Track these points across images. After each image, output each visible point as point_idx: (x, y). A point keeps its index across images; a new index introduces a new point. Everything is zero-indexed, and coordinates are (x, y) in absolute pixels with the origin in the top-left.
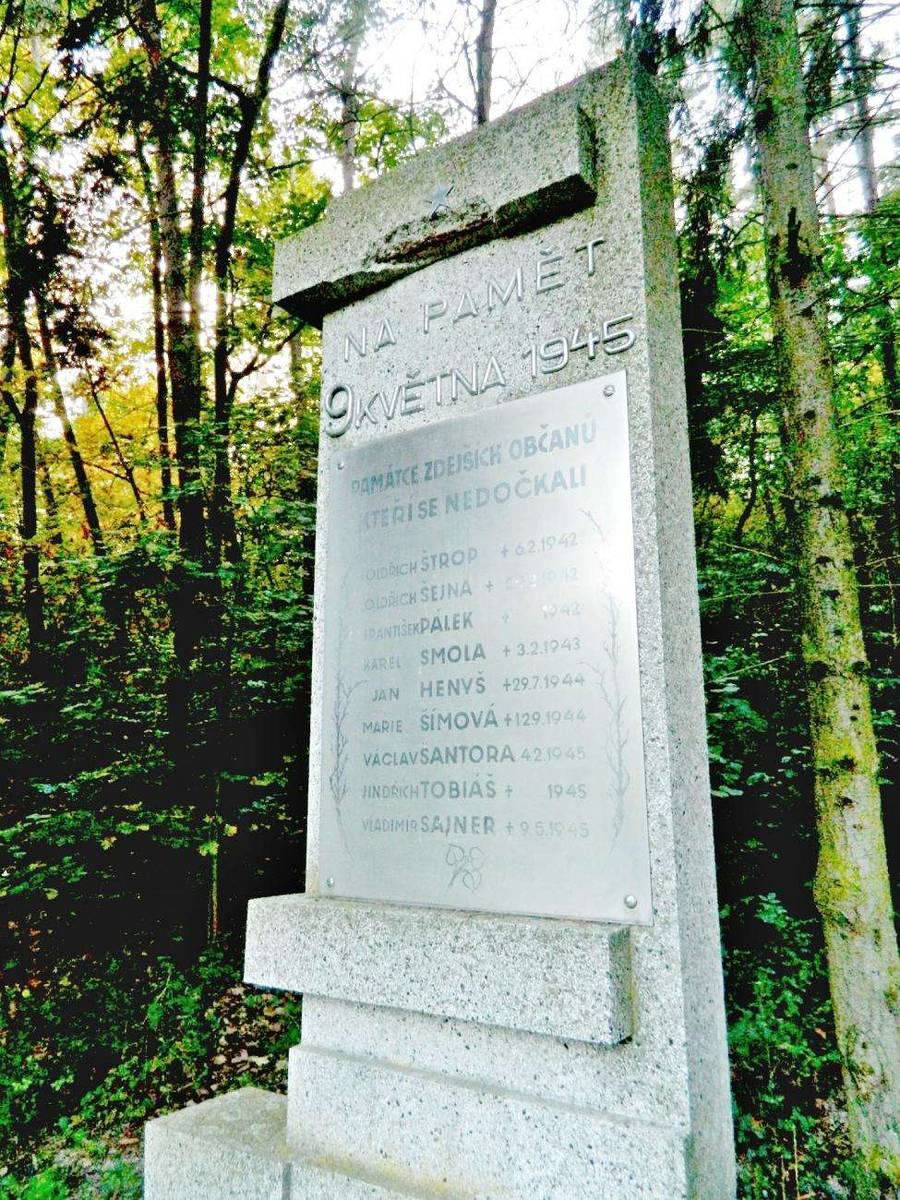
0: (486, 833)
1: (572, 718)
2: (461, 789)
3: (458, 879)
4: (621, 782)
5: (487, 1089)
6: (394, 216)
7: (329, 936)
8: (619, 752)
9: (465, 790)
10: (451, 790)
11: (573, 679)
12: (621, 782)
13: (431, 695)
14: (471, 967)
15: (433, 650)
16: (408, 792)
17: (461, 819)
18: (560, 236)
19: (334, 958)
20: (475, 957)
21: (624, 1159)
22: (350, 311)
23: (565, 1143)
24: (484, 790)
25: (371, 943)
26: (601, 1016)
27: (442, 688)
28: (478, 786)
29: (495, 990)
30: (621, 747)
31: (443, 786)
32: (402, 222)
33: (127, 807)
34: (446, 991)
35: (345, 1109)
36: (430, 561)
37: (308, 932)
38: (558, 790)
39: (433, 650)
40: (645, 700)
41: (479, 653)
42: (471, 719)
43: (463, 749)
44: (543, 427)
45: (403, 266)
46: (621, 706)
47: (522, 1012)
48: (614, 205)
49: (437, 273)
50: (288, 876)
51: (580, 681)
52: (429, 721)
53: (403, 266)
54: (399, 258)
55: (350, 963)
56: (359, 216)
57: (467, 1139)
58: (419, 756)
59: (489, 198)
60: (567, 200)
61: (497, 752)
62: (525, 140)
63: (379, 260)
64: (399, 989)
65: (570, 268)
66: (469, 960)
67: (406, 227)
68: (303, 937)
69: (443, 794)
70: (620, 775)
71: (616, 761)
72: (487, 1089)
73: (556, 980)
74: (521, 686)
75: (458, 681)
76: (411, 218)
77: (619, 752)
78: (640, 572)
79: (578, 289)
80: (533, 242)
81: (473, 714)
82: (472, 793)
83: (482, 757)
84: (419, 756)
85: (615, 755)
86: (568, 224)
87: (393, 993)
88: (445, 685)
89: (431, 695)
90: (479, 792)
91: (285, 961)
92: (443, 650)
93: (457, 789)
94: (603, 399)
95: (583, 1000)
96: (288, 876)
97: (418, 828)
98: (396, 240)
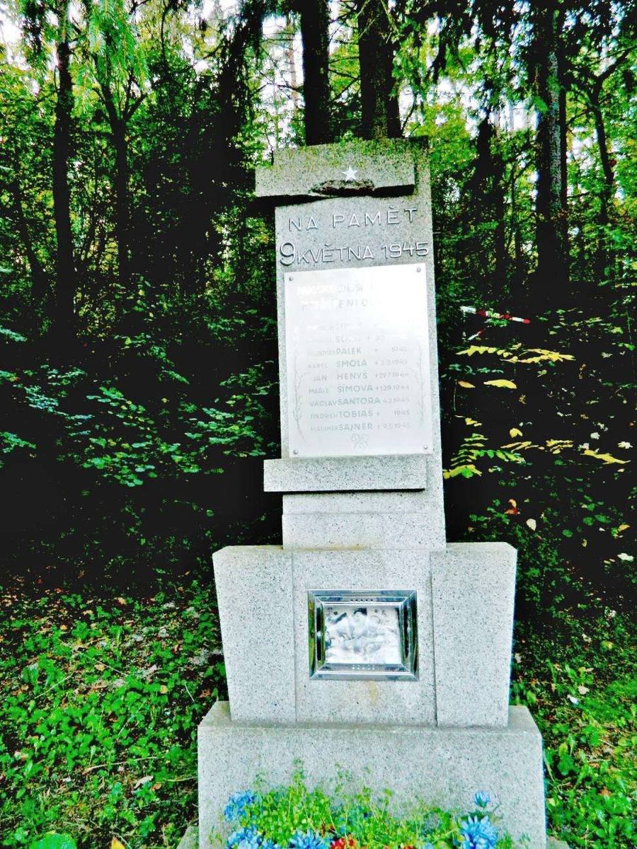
5: (371, 514)
6: (326, 174)
18: (398, 203)
19: (311, 477)
21: (425, 523)
22: (290, 208)
23: (404, 522)
32: (331, 179)
33: (569, 357)
35: (312, 531)
40: (432, 381)
41: (364, 363)
43: (358, 399)
45: (323, 196)
46: (423, 384)
48: (420, 197)
49: (338, 201)
50: (276, 453)
53: (323, 196)
54: (324, 192)
56: (306, 169)
57: (367, 530)
59: (375, 182)
60: (407, 191)
62: (391, 162)
63: (314, 191)
65: (403, 218)
66: (372, 469)
67: (332, 181)
70: (422, 407)
72: (371, 514)
76: (335, 179)
78: (430, 338)
79: (405, 227)
80: (385, 202)
86: (401, 199)
88: (349, 375)
94: (417, 273)
96: (276, 453)
98: (325, 186)
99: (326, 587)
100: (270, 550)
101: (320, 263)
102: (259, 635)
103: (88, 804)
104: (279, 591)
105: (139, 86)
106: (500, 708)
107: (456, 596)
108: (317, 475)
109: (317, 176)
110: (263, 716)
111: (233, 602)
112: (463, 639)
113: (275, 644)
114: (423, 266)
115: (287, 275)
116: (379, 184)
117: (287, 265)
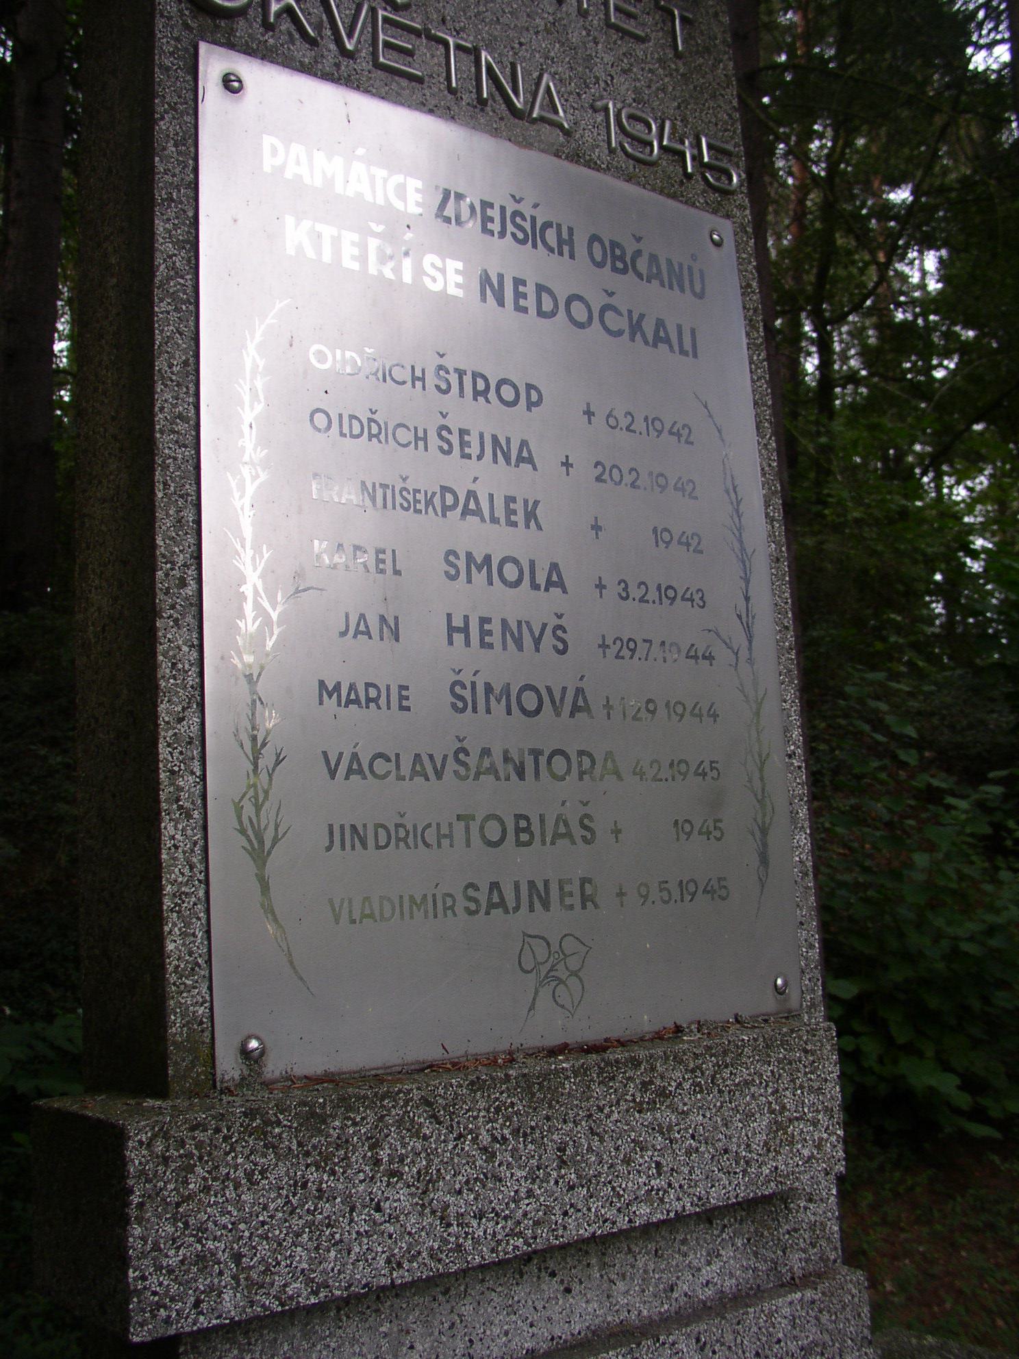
0: (584, 907)
1: (701, 716)
2: (536, 827)
3: (545, 993)
4: (764, 815)
7: (384, 1154)
8: (761, 770)
9: (543, 834)
10: (518, 830)
11: (700, 654)
12: (764, 815)
13: (468, 643)
14: (670, 1128)
15: (469, 556)
16: (431, 836)
17: (541, 886)
19: (401, 1197)
20: (674, 1110)
24: (578, 832)
25: (485, 1138)
26: (834, 1139)
27: (490, 633)
28: (566, 824)
29: (707, 1151)
30: (763, 763)
31: (502, 823)
34: (633, 1183)
36: (454, 379)
37: (327, 1158)
38: (524, 837)
39: (469, 556)
42: (546, 698)
44: (639, 240)
47: (745, 1172)
51: (709, 658)
52: (467, 694)
55: (439, 1195)
58: (451, 765)
61: (593, 762)
64: (548, 1210)
68: (313, 1174)
69: (503, 839)
71: (757, 784)
73: (783, 1108)
74: (625, 652)
75: (519, 623)
77: (761, 770)
81: (549, 689)
82: (556, 836)
83: (569, 771)
84: (451, 765)
85: (757, 775)
87: (537, 1223)
89: (468, 643)
90: (568, 835)
91: (264, 1248)
92: (488, 559)
93: (527, 830)
95: (815, 1123)
97: (459, 909)
108: (426, 1181)
115: (214, 63)
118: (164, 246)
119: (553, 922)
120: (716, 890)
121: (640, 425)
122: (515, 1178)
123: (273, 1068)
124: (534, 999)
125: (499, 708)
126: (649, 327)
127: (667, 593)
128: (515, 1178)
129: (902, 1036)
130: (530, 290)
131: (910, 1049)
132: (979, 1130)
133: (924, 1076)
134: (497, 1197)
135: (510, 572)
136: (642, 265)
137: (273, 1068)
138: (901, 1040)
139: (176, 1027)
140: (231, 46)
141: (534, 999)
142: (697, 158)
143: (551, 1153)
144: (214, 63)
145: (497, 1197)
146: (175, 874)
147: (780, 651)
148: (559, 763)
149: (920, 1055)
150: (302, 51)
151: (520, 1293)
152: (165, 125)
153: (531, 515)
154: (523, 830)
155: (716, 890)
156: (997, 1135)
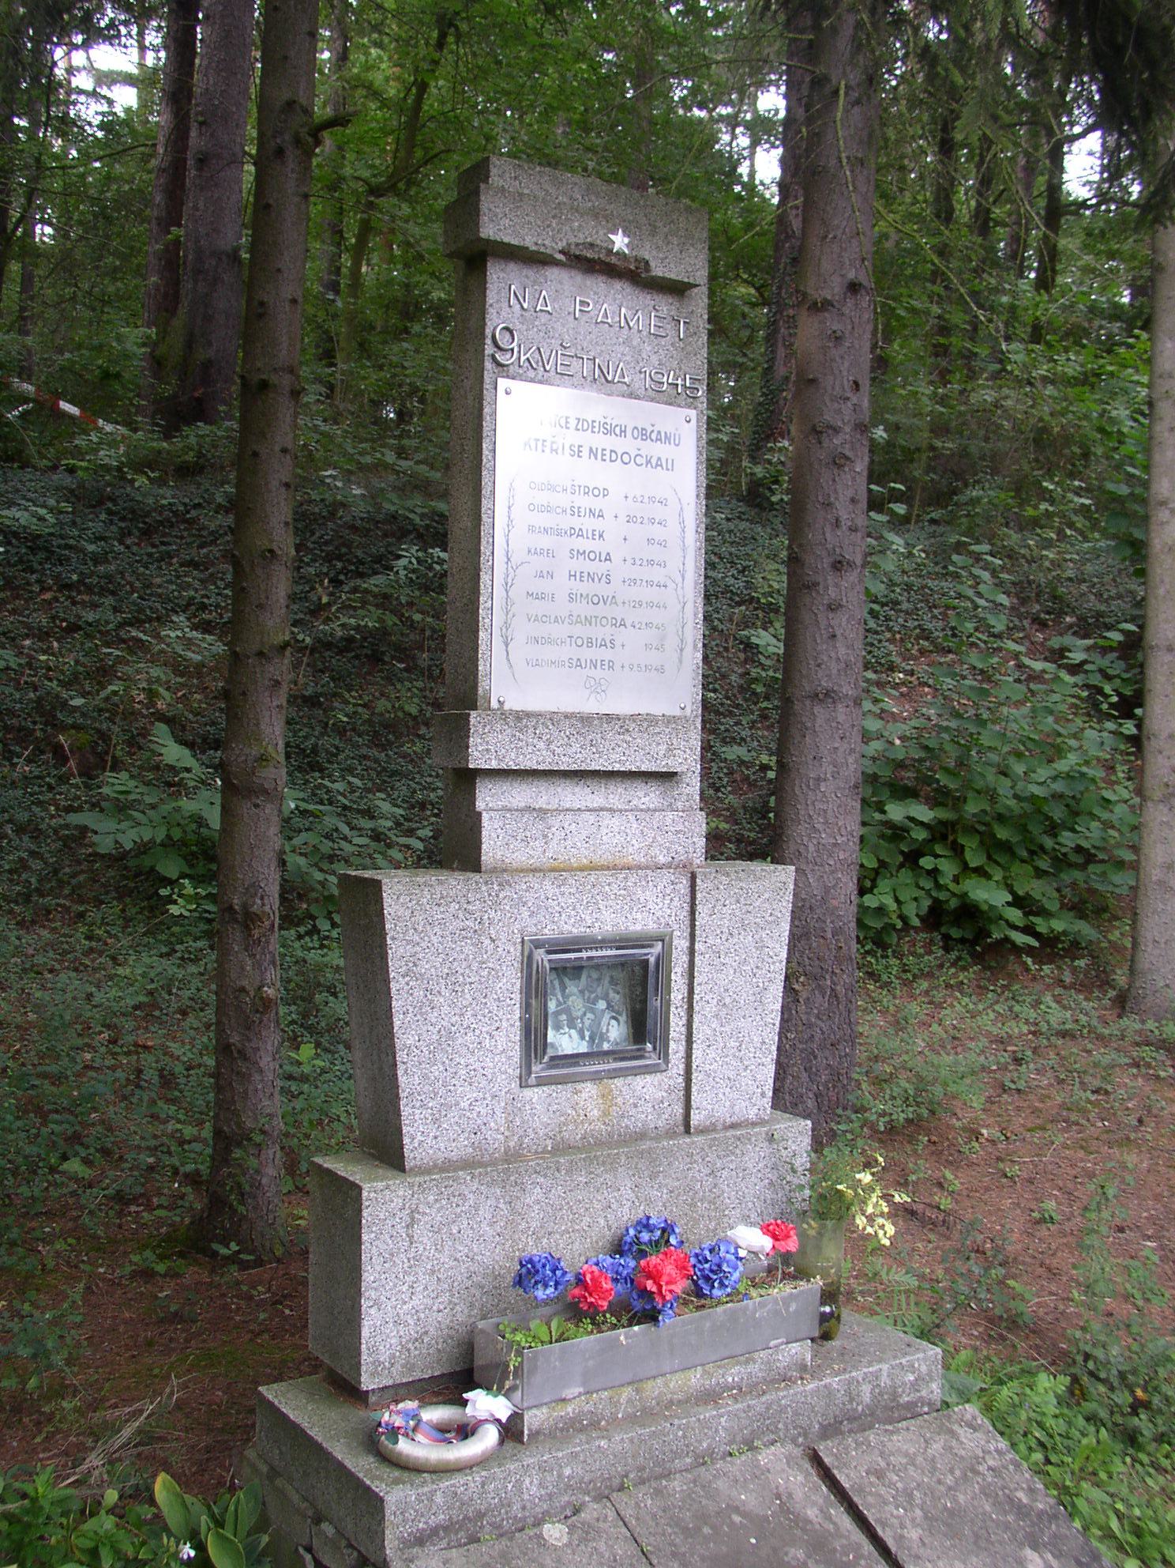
19: (541, 745)
41: (608, 558)
99: (549, 933)
100: (453, 883)
101: (553, 373)
102: (454, 1019)
103: (1052, 414)
104: (487, 942)
105: (423, 87)
106: (763, 1095)
107: (724, 937)
108: (549, 742)
109: (573, 230)
110: (454, 1156)
111: (415, 965)
112: (728, 1000)
113: (477, 1032)
114: (693, 413)
115: (503, 383)
116: (658, 271)
117: (503, 366)
118: (485, 452)
119: (598, 673)
120: (661, 670)
121: (646, 500)
122: (576, 747)
123: (506, 707)
124: (693, 912)
125: (584, 602)
126: (654, 461)
127: (651, 562)
128: (576, 747)
129: (974, 859)
130: (607, 453)
131: (980, 872)
132: (1020, 939)
133: (989, 894)
134: (570, 751)
135: (592, 556)
136: (654, 436)
137: (506, 707)
138: (973, 864)
139: (480, 691)
140: (508, 377)
141: (693, 912)
142: (684, 386)
143: (588, 742)
144: (503, 383)
145: (570, 751)
146: (482, 648)
147: (696, 583)
148: (604, 621)
149: (987, 876)
150: (531, 374)
151: (577, 790)
152: (486, 410)
153: (601, 536)
154: (590, 643)
155: (661, 670)
156: (1036, 944)
